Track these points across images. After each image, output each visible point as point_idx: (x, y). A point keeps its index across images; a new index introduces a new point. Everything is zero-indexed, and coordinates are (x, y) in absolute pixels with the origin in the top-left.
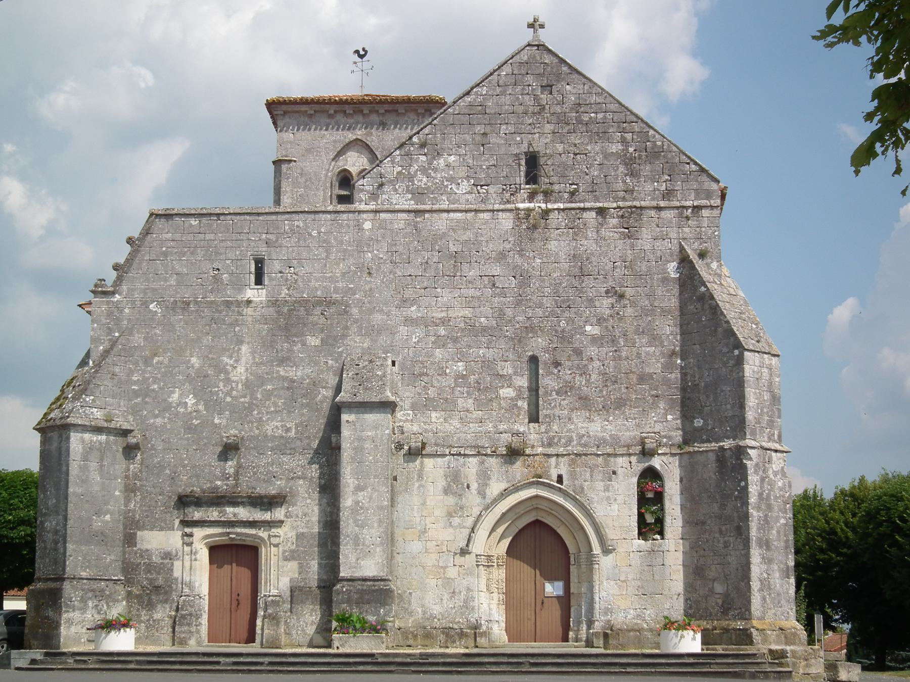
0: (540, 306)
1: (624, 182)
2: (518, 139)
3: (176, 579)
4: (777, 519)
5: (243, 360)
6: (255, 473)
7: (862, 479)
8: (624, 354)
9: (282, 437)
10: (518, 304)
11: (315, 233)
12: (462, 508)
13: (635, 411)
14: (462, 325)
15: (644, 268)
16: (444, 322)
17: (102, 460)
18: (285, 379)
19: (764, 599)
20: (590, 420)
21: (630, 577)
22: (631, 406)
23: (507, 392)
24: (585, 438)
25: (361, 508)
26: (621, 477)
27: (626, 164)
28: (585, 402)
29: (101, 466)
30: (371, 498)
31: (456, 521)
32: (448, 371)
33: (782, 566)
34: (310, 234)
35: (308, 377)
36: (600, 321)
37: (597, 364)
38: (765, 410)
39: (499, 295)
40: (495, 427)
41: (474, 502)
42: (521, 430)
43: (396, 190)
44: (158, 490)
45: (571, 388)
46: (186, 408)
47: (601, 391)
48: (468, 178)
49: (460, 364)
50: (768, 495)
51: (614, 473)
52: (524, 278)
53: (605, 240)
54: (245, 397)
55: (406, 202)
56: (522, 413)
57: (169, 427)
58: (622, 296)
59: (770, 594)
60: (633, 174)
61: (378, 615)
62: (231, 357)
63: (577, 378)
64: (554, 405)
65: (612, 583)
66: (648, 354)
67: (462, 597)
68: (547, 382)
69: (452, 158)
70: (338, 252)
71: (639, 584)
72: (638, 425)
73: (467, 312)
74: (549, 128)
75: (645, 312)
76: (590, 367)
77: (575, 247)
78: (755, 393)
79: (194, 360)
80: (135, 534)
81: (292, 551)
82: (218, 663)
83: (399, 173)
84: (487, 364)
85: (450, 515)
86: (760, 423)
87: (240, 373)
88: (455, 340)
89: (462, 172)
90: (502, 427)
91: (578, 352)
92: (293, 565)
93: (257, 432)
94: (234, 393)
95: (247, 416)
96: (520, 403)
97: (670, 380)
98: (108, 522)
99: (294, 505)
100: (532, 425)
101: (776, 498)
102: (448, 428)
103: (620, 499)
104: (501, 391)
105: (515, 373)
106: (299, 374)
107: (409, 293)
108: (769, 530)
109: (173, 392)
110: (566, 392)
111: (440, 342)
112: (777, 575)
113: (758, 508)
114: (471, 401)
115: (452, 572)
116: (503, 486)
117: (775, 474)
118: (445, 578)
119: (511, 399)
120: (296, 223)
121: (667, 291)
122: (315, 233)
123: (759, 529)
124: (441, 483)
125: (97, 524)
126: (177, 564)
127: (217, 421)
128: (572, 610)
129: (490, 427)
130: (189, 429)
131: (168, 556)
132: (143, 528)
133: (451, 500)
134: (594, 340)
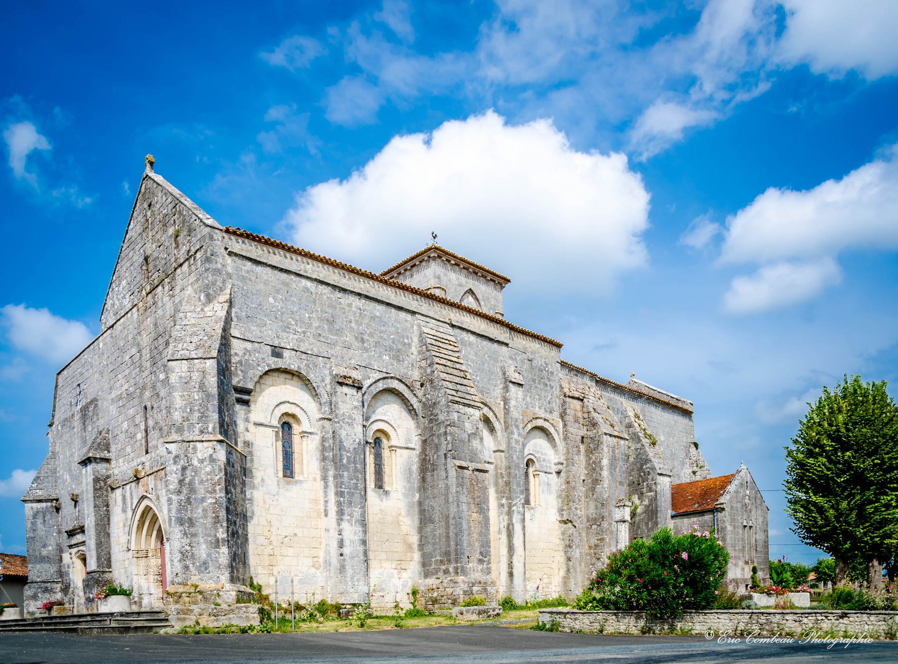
4: (203, 500)
33: (210, 539)
38: (196, 408)
59: (194, 563)
78: (181, 396)
101: (201, 482)
112: (204, 546)
117: (202, 461)
123: (179, 511)
125: (44, 552)
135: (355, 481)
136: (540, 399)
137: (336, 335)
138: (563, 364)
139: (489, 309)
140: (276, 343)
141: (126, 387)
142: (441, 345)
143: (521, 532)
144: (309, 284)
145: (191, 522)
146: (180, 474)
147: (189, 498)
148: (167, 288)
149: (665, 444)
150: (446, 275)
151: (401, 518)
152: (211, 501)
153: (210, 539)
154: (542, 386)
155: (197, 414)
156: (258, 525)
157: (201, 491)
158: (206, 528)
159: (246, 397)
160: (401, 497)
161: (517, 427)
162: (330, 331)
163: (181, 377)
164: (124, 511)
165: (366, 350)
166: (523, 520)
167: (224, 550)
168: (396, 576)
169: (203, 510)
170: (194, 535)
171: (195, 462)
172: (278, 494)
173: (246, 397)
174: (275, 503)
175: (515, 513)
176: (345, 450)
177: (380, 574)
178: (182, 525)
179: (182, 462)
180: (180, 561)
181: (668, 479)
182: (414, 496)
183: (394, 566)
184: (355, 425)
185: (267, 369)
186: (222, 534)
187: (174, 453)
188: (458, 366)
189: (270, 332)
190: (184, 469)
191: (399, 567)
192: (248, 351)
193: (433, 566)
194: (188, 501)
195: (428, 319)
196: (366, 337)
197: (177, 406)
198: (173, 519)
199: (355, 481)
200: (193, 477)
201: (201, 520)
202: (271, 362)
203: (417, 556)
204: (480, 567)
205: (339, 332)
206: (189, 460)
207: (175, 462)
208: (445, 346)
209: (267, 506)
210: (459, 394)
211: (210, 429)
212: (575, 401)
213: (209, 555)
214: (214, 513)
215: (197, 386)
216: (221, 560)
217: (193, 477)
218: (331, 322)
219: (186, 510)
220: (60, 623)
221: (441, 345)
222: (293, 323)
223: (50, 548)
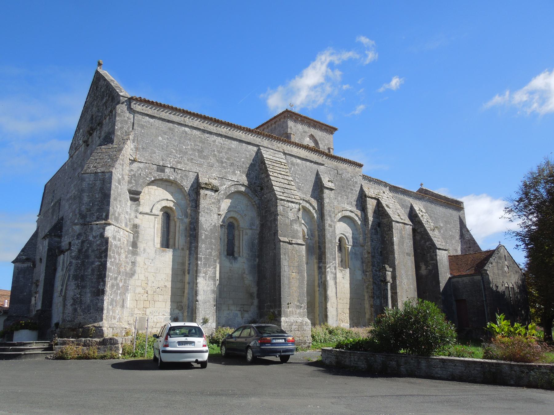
4: (93, 263)
19: (75, 310)
33: (94, 289)
38: (96, 203)
50: (87, 250)
101: (93, 251)
108: (84, 270)
112: (89, 295)
117: (94, 237)
123: (76, 270)
135: (210, 250)
136: (347, 198)
137: (204, 159)
138: (365, 177)
139: (324, 146)
140: (161, 164)
141: (74, 191)
142: (275, 164)
143: (334, 286)
144: (187, 129)
148: (98, 132)
149: (444, 229)
150: (295, 126)
151: (245, 276)
153: (94, 289)
154: (349, 190)
155: (96, 207)
156: (138, 279)
157: (92, 258)
158: (92, 282)
159: (137, 196)
160: (246, 261)
161: (330, 216)
162: (200, 157)
164: (62, 270)
165: (224, 168)
166: (335, 278)
168: (239, 315)
169: (92, 270)
170: (84, 287)
171: (91, 238)
172: (155, 258)
173: (137, 196)
174: (152, 265)
175: (330, 273)
176: (204, 230)
177: (228, 314)
178: (76, 280)
180: (72, 305)
181: (446, 252)
182: (255, 261)
183: (238, 309)
184: (212, 214)
185: (153, 179)
187: (78, 232)
188: (287, 178)
189: (158, 157)
190: (83, 242)
191: (242, 309)
192: (140, 168)
194: (83, 263)
195: (267, 150)
196: (224, 160)
197: (84, 202)
198: (71, 276)
199: (210, 250)
200: (88, 248)
202: (156, 175)
203: (256, 302)
204: (298, 311)
205: (205, 157)
206: (87, 236)
207: (78, 238)
208: (277, 165)
209: (146, 267)
210: (285, 195)
211: (104, 217)
212: (373, 200)
213: (92, 301)
215: (98, 189)
217: (88, 248)
218: (201, 151)
219: (81, 270)
221: (275, 164)
222: (174, 151)
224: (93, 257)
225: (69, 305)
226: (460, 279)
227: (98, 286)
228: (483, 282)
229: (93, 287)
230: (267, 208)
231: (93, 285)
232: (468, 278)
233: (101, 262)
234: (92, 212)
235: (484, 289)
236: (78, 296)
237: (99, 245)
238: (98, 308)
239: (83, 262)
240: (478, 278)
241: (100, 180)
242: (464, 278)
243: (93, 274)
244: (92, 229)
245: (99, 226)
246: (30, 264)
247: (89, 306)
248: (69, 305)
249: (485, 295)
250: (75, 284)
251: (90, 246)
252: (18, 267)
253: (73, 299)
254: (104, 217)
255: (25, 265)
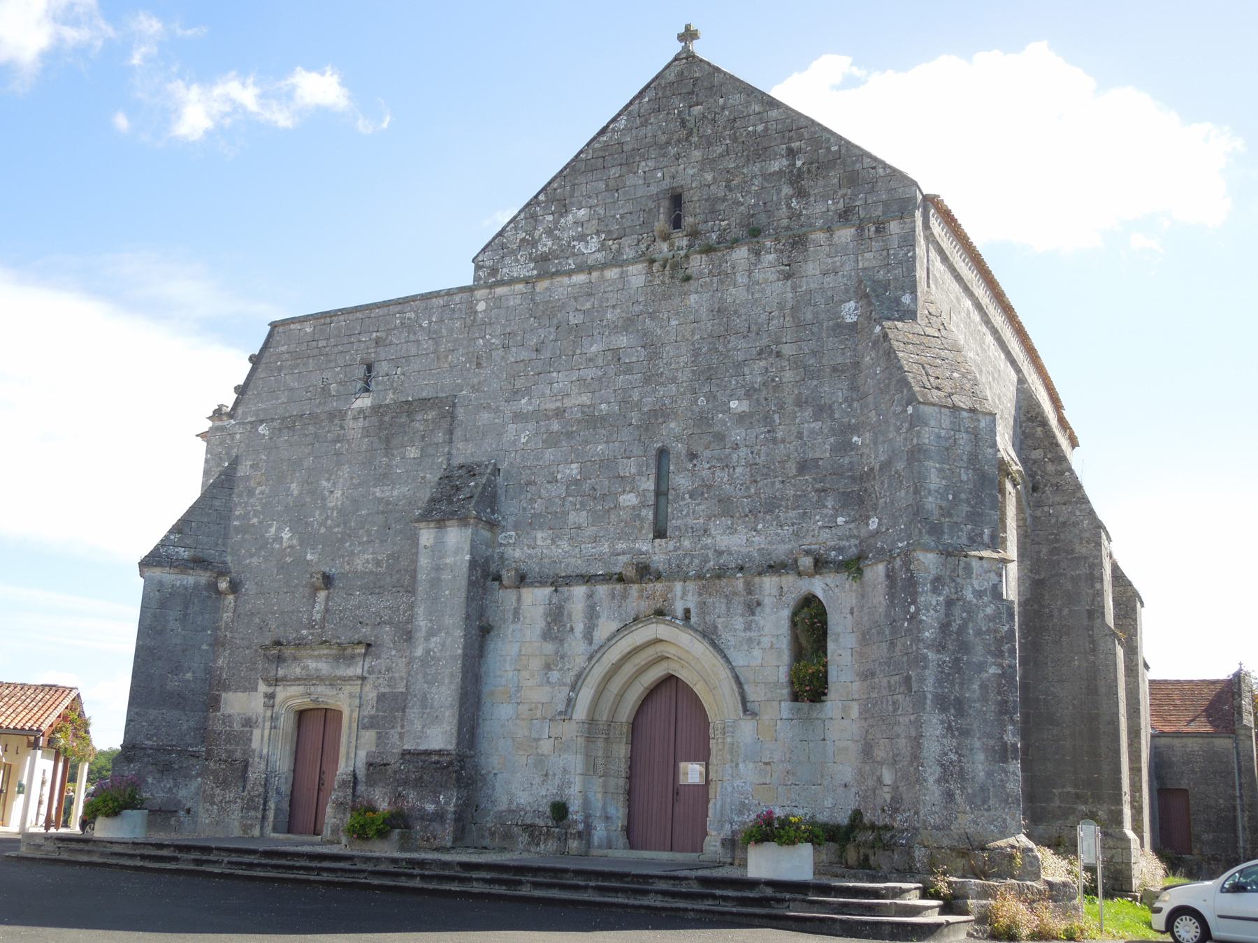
0: (674, 380)
1: (789, 207)
2: (659, 175)
3: (254, 751)
4: (981, 667)
5: (340, 485)
6: (341, 619)
7: (202, 436)
8: (779, 435)
9: (372, 572)
10: (647, 380)
11: (425, 324)
12: (562, 657)
13: (792, 514)
14: (579, 415)
15: (809, 316)
16: (559, 413)
17: (186, 607)
18: (380, 500)
19: (950, 796)
20: (732, 530)
21: (776, 757)
22: (787, 508)
23: (629, 499)
24: (725, 556)
25: (433, 658)
26: (768, 610)
27: (792, 184)
28: (725, 506)
29: (185, 615)
30: (443, 645)
31: (555, 675)
32: (559, 476)
33: (992, 742)
34: (421, 326)
35: (404, 496)
36: (750, 392)
37: (743, 452)
38: (963, 496)
39: (625, 373)
40: (612, 546)
41: (577, 647)
42: (644, 549)
43: (517, 261)
44: (246, 643)
45: (709, 487)
46: (281, 544)
47: (748, 488)
48: (598, 233)
49: (574, 466)
50: (962, 630)
51: (759, 604)
52: (653, 348)
53: (758, 283)
54: (338, 526)
55: (528, 270)
56: (646, 526)
57: (263, 566)
58: (778, 355)
59: (963, 788)
60: (802, 194)
61: (438, 803)
62: (328, 480)
63: (718, 473)
64: (683, 514)
65: (751, 765)
66: (812, 431)
67: (557, 781)
68: (681, 481)
69: (582, 212)
70: (447, 342)
71: (789, 767)
72: (796, 534)
73: (585, 399)
74: (697, 154)
75: (810, 374)
76: (735, 456)
77: (721, 298)
78: (941, 470)
79: (294, 486)
80: (220, 696)
81: (372, 717)
82: (175, 859)
83: (523, 240)
84: (607, 464)
85: (548, 667)
86: (950, 515)
87: (336, 498)
88: (569, 435)
89: (592, 227)
90: (620, 546)
91: (720, 438)
92: (369, 736)
93: (347, 567)
94: (329, 522)
95: (339, 549)
96: (644, 512)
97: (841, 466)
98: (188, 681)
99: (378, 657)
100: (657, 541)
101: (979, 633)
102: (556, 552)
103: (766, 641)
104: (621, 498)
105: (640, 474)
106: (395, 493)
107: (520, 383)
108: (962, 684)
109: (271, 526)
110: (703, 494)
111: (552, 441)
112: (981, 757)
113: (940, 647)
114: (584, 513)
115: (546, 746)
116: (614, 626)
117: (979, 594)
118: (537, 754)
119: (634, 508)
120: (408, 315)
121: (841, 342)
122: (425, 324)
123: (939, 682)
124: (541, 624)
125: (173, 684)
126: (257, 733)
127: (309, 557)
128: (710, 805)
129: (605, 548)
130: (282, 567)
131: (249, 723)
132: (226, 688)
133: (549, 648)
134: (741, 418)
145: (960, 706)
146: (943, 611)
147: (957, 660)
152: (993, 670)
153: (992, 742)
155: (965, 508)
157: (978, 654)
158: (985, 720)
163: (939, 437)
167: (1016, 766)
169: (981, 687)
170: (965, 733)
171: (969, 595)
179: (946, 591)
180: (938, 781)
186: (1012, 737)
190: (950, 603)
193: (1057, 803)
201: (977, 705)
206: (959, 589)
211: (986, 538)
213: (989, 774)
214: (999, 693)
215: (965, 457)
216: (1010, 785)
219: (952, 683)
220: (81, 851)
223: (189, 676)
224: (980, 649)
225: (931, 780)
226: (1177, 742)
227: (1001, 734)
228: (1238, 754)
229: (989, 736)
230: (1057, 541)
231: (988, 729)
232: (1200, 741)
233: (1000, 665)
234: (955, 519)
235: (1239, 769)
236: (954, 757)
237: (990, 619)
238: (1008, 795)
239: (957, 661)
240: (1224, 743)
241: (967, 432)
242: (1189, 741)
243: (984, 699)
244: (968, 569)
245: (985, 564)
246: (203, 577)
247: (983, 789)
248: (931, 780)
249: (1240, 785)
250: (942, 722)
251: (971, 618)
252: (161, 583)
253: (942, 765)
254: (986, 538)
255: (190, 579)
